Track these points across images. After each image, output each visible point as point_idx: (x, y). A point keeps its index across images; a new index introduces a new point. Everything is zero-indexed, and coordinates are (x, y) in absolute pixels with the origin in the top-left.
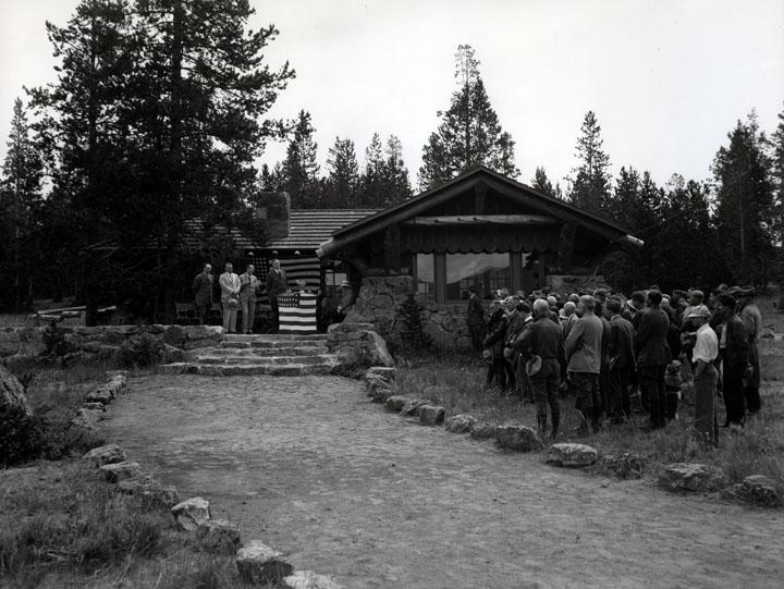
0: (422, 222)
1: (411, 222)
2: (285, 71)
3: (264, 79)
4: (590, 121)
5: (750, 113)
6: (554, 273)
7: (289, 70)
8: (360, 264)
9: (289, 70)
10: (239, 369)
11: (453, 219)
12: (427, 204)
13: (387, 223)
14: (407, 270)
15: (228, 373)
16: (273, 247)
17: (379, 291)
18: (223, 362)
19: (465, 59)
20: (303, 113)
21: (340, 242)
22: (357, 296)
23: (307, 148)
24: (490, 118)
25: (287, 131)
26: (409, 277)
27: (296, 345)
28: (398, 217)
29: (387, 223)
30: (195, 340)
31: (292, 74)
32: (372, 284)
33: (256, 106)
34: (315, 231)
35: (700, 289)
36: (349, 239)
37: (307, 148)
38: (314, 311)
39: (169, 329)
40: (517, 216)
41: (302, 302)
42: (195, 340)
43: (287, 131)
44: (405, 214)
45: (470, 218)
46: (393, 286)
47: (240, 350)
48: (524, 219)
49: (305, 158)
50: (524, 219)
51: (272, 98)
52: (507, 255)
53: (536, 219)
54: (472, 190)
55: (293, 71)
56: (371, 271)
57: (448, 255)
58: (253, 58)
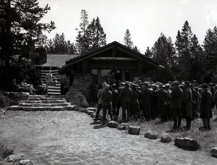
0: (95, 59)
1: (92, 59)
2: (47, 7)
3: (39, 10)
4: (128, 32)
5: (161, 33)
6: (135, 76)
7: (48, 7)
8: (72, 72)
9: (48, 7)
10: (39, 108)
11: (105, 58)
12: (97, 53)
13: (84, 59)
14: (89, 74)
15: (35, 110)
16: (42, 66)
17: (81, 81)
18: (31, 106)
19: (84, 14)
20: (52, 22)
21: (68, 65)
22: (72, 83)
23: (41, 36)
24: (101, 29)
25: (47, 27)
26: (90, 77)
27: (56, 99)
28: (88, 57)
29: (84, 59)
30: (19, 97)
31: (49, 9)
32: (78, 79)
33: (37, 19)
34: (57, 61)
35: (141, 80)
36: (72, 64)
37: (41, 36)
38: (60, 87)
39: (10, 93)
40: (125, 58)
41: (56, 85)
42: (19, 97)
43: (47, 27)
44: (90, 56)
45: (111, 58)
46: (85, 80)
47: (36, 101)
48: (128, 59)
49: (40, 39)
50: (128, 59)
51: (41, 16)
52: (97, 70)
53: (131, 59)
54: (111, 49)
55: (49, 7)
56: (78, 74)
57: (102, 70)
58: (36, 2)
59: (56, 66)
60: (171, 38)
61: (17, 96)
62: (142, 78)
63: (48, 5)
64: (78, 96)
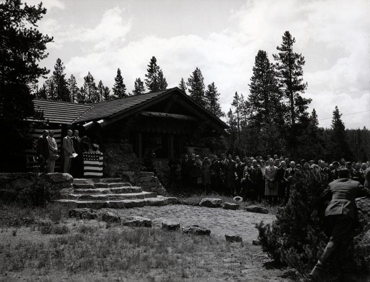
7: (42, 7)
11: (157, 114)
30: (57, 183)
40: (183, 116)
42: (57, 183)
45: (164, 114)
59: (58, 122)
60: (74, 77)
61: (54, 180)
62: (199, 149)
63: (41, 4)
64: (151, 179)
